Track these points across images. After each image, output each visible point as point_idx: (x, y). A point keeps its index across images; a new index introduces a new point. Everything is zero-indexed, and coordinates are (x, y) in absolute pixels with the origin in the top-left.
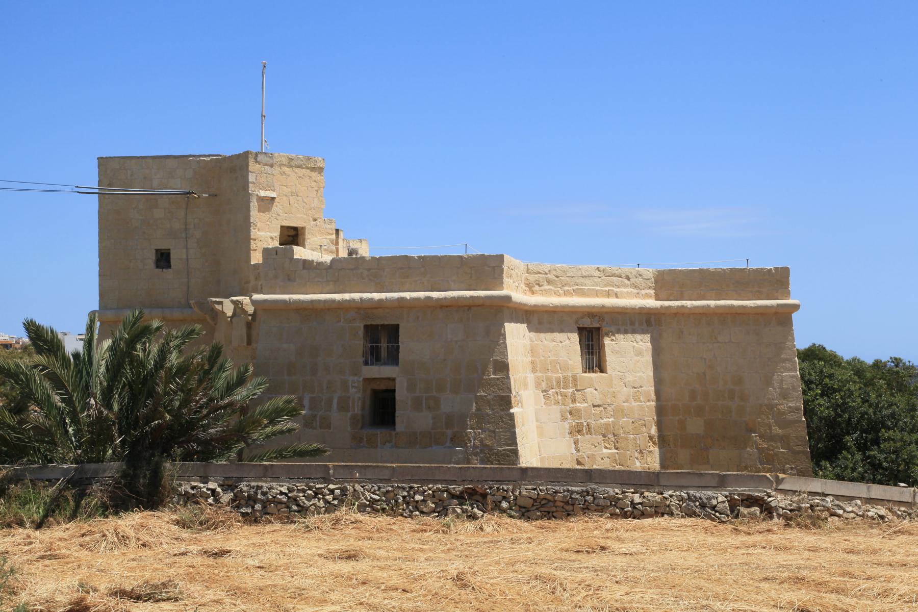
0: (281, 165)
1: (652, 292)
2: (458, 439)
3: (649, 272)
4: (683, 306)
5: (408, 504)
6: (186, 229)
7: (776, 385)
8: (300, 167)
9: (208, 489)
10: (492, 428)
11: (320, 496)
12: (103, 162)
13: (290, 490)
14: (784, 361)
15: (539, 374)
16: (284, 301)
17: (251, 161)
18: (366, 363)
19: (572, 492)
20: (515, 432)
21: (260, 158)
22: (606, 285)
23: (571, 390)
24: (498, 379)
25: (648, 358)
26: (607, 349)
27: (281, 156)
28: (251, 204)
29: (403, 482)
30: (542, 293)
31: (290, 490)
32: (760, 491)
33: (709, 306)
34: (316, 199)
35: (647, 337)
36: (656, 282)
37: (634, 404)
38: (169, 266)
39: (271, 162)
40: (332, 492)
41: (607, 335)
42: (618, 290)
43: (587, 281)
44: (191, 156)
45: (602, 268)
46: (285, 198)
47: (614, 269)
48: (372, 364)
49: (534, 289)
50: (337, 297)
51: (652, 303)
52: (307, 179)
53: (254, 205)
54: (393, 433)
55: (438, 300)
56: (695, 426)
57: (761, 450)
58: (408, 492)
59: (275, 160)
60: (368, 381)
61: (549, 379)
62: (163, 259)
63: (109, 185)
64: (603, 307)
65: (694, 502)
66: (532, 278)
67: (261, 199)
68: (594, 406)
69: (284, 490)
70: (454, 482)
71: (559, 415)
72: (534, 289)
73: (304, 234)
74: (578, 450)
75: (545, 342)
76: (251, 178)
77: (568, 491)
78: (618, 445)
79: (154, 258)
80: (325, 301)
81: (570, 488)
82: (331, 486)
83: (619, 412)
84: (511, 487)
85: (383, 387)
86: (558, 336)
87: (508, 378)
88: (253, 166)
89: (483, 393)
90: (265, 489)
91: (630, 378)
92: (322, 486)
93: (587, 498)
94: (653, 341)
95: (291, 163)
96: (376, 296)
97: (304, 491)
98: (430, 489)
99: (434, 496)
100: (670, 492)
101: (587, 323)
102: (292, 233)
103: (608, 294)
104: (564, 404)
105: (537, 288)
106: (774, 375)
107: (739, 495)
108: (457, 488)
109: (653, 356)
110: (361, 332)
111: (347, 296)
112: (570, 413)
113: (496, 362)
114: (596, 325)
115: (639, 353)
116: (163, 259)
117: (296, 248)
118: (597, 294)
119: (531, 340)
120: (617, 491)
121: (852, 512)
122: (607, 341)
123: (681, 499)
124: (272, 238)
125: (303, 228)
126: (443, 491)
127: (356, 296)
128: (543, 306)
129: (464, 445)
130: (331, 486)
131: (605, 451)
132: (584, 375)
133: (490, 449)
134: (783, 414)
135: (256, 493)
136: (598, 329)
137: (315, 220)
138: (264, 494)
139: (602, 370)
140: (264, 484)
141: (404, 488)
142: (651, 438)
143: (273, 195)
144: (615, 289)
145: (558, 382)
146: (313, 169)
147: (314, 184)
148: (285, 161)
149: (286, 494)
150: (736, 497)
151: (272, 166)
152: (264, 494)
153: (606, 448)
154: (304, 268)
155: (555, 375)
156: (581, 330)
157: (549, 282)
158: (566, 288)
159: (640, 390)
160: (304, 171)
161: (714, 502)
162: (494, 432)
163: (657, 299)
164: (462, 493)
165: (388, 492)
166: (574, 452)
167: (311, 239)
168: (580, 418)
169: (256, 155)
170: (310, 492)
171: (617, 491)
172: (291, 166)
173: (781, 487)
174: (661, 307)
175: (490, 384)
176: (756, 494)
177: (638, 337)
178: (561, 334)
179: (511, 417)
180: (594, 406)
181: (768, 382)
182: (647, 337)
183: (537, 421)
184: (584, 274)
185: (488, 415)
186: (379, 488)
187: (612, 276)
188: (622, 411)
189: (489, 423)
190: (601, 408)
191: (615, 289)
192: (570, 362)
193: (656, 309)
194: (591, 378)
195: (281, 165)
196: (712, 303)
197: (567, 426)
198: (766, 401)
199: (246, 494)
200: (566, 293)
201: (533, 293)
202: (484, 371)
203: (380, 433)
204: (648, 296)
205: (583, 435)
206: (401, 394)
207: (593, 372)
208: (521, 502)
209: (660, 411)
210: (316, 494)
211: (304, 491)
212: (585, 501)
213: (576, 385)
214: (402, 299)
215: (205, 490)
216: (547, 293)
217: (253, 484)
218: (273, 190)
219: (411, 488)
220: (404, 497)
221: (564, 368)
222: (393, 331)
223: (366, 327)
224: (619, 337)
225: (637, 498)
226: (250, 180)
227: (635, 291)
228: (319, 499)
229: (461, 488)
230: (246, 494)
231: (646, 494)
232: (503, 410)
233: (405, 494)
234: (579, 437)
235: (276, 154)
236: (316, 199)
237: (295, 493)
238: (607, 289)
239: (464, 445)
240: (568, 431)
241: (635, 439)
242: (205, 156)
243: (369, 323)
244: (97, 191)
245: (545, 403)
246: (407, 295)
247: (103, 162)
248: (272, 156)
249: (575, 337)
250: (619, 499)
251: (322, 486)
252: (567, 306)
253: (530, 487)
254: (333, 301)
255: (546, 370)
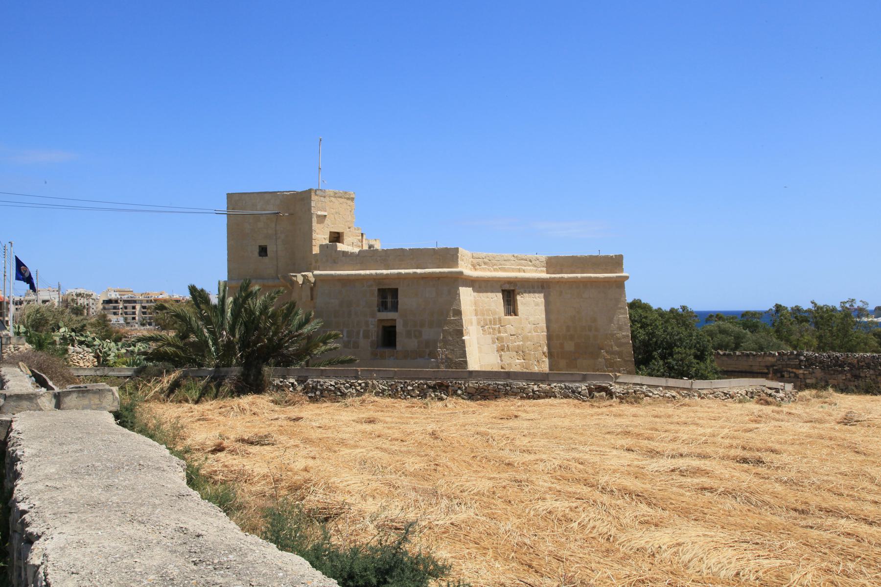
0: (330, 196)
1: (545, 269)
2: (433, 354)
3: (543, 257)
4: (562, 277)
5: (404, 391)
6: (276, 234)
7: (616, 322)
8: (341, 197)
9: (290, 383)
10: (452, 348)
11: (353, 387)
12: (230, 196)
13: (336, 383)
14: (620, 308)
15: (479, 317)
16: (332, 275)
17: (313, 194)
18: (379, 311)
19: (499, 385)
20: (465, 351)
21: (318, 192)
22: (518, 265)
23: (498, 326)
24: (455, 320)
25: (542, 307)
26: (519, 303)
27: (330, 191)
28: (313, 219)
29: (401, 379)
30: (481, 270)
31: (336, 383)
32: (605, 383)
33: (577, 277)
34: (350, 216)
35: (542, 295)
36: (547, 263)
37: (534, 334)
38: (266, 255)
39: (324, 195)
40: (360, 384)
41: (519, 294)
42: (525, 268)
43: (507, 263)
44: (278, 192)
45: (516, 255)
46: (332, 215)
47: (523, 256)
48: (383, 311)
49: (476, 267)
50: (362, 272)
51: (545, 276)
52: (345, 205)
53: (314, 219)
54: (395, 351)
55: (421, 274)
56: (569, 346)
57: (606, 360)
58: (404, 385)
59: (326, 194)
60: (381, 321)
61: (485, 320)
62: (263, 251)
63: (233, 209)
64: (516, 278)
65: (568, 390)
66: (475, 261)
67: (318, 216)
68: (511, 335)
69: (333, 383)
70: (430, 379)
71: (491, 341)
72: (476, 267)
73: (343, 236)
74: (501, 361)
75: (483, 298)
76: (313, 204)
77: (496, 384)
78: (525, 358)
79: (258, 251)
80: (355, 275)
81: (497, 382)
82: (360, 382)
83: (526, 338)
84: (463, 382)
85: (388, 324)
86: (490, 295)
87: (461, 319)
88: (314, 197)
89: (446, 328)
90: (322, 383)
91: (532, 319)
92: (354, 381)
93: (507, 388)
94: (546, 298)
95: (335, 195)
96: (385, 272)
97: (344, 384)
98: (416, 383)
99: (419, 387)
100: (555, 384)
101: (507, 287)
102: (336, 235)
103: (519, 270)
104: (493, 334)
105: (478, 267)
106: (614, 317)
107: (594, 385)
108: (432, 383)
109: (545, 306)
110: (376, 293)
111: (368, 272)
112: (497, 339)
113: (454, 309)
114: (512, 288)
115: (537, 305)
116: (263, 251)
117: (338, 244)
118: (513, 270)
119: (475, 297)
120: (524, 384)
121: (657, 394)
122: (519, 298)
123: (561, 388)
124: (325, 239)
125: (343, 233)
126: (424, 384)
127: (373, 272)
128: (481, 277)
129: (436, 358)
130: (360, 382)
131: (517, 361)
132: (507, 317)
133: (451, 360)
134: (619, 339)
135: (317, 385)
136: (513, 291)
137: (349, 228)
138: (321, 385)
139: (516, 315)
140: (322, 381)
141: (401, 383)
142: (544, 353)
143: (325, 214)
144: (523, 268)
145: (490, 321)
146: (348, 199)
147: (349, 207)
148: (332, 194)
149: (334, 386)
150: (592, 387)
151: (325, 197)
152: (321, 385)
153: (518, 359)
154: (343, 256)
155: (488, 318)
156: (504, 292)
157: (485, 263)
158: (495, 267)
159: (538, 325)
160: (343, 200)
161: (580, 390)
162: (453, 350)
163: (547, 273)
164: (435, 385)
165: (392, 385)
166: (500, 362)
167: (347, 239)
168: (503, 342)
169: (316, 191)
170: (347, 385)
171: (524, 384)
172: (336, 197)
173: (617, 381)
174: (550, 278)
175: (451, 322)
176: (604, 385)
177: (537, 295)
178: (492, 294)
179: (463, 342)
180: (511, 335)
181: (611, 321)
182: (542, 295)
183: (478, 344)
184: (506, 258)
185: (449, 340)
186: (387, 382)
187: (522, 259)
188: (527, 338)
189: (450, 345)
190: (515, 336)
191: (523, 268)
192: (497, 310)
193: (547, 279)
194: (509, 319)
195: (330, 196)
196: (579, 275)
197: (495, 347)
198: (610, 332)
199: (311, 386)
200: (495, 270)
201: (476, 270)
202: (447, 315)
203: (387, 351)
204: (542, 271)
205: (505, 352)
206: (399, 328)
207: (511, 315)
208: (469, 390)
209: (549, 338)
210: (351, 386)
211: (344, 384)
212: (506, 390)
213: (500, 323)
214: (400, 274)
215: (288, 383)
216: (484, 270)
217: (315, 380)
218: (325, 211)
219: (405, 382)
220: (401, 388)
221: (494, 313)
222: (395, 292)
223: (379, 290)
224: (526, 295)
225: (536, 388)
226: (312, 205)
227: (535, 268)
228: (353, 389)
229: (434, 382)
230: (311, 386)
231: (541, 385)
232: (458, 338)
233: (402, 386)
234: (503, 353)
235: (327, 190)
236: (350, 216)
237: (339, 385)
238: (518, 267)
239: (436, 358)
240: (496, 350)
241: (535, 354)
242: (287, 192)
243: (381, 288)
244: (226, 212)
245: (483, 334)
246: (403, 271)
247: (230, 196)
248: (325, 191)
249: (500, 295)
250: (525, 388)
251: (354, 381)
252: (496, 277)
253: (474, 382)
254: (360, 275)
255: (483, 314)
